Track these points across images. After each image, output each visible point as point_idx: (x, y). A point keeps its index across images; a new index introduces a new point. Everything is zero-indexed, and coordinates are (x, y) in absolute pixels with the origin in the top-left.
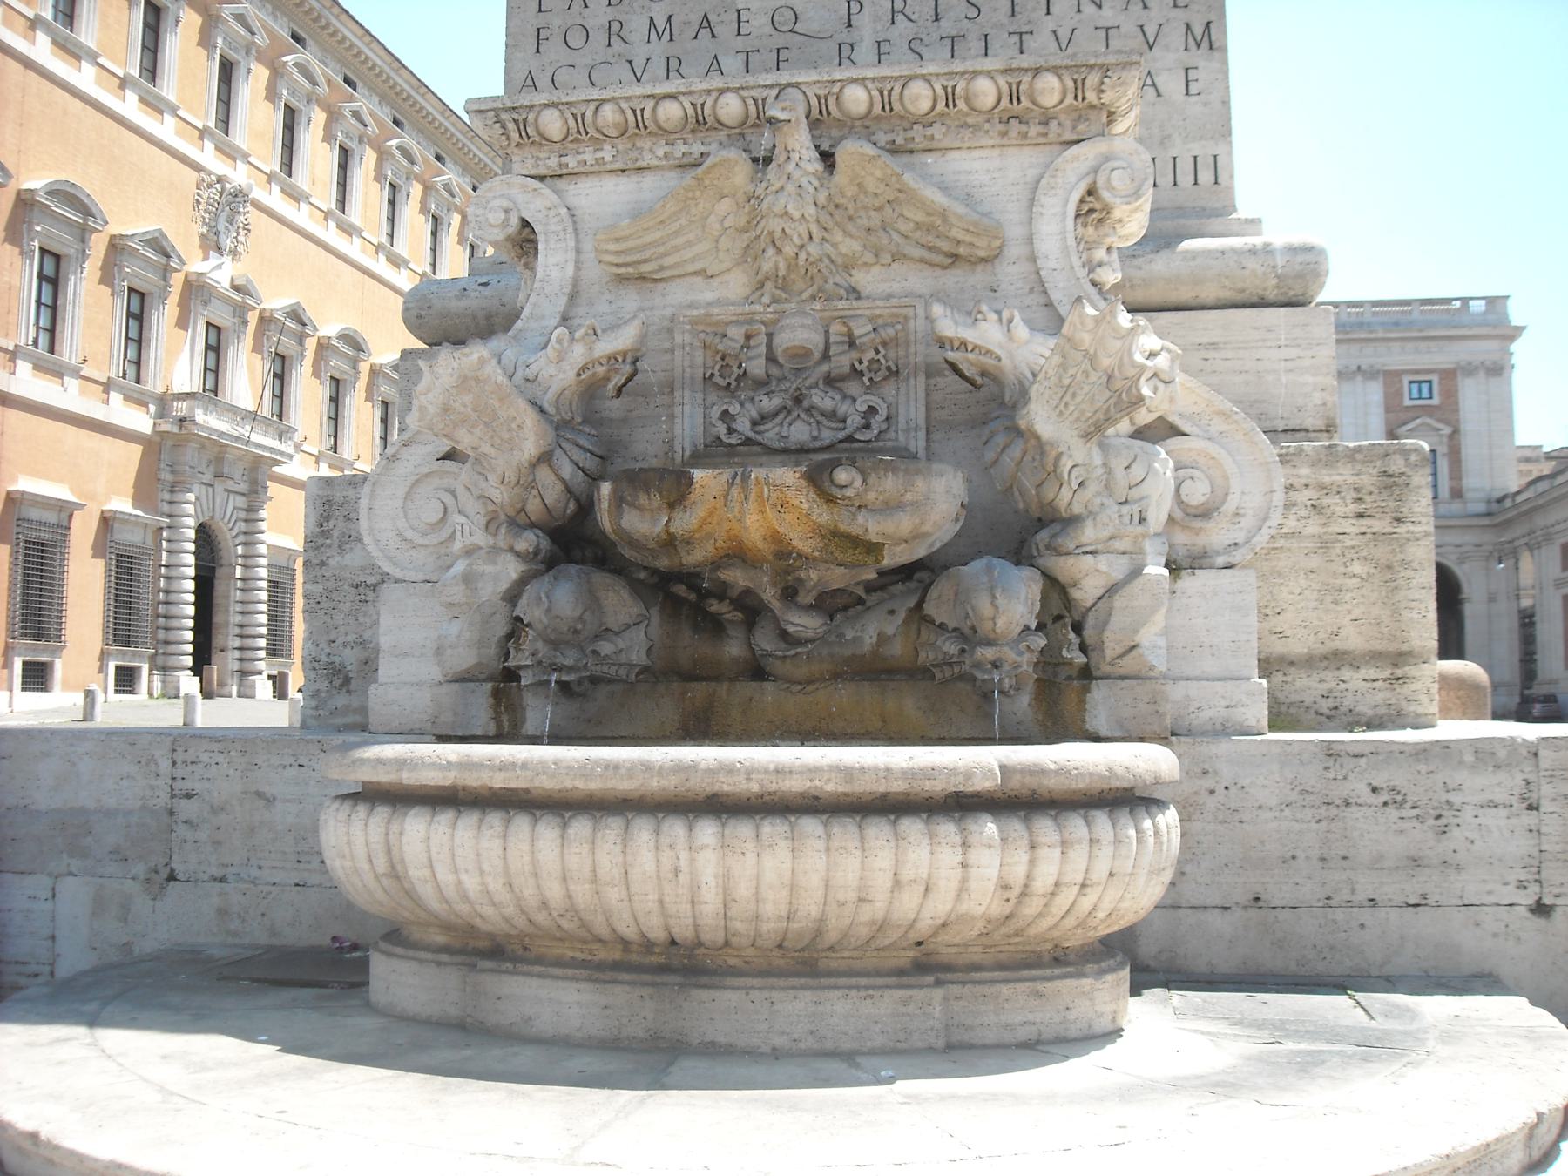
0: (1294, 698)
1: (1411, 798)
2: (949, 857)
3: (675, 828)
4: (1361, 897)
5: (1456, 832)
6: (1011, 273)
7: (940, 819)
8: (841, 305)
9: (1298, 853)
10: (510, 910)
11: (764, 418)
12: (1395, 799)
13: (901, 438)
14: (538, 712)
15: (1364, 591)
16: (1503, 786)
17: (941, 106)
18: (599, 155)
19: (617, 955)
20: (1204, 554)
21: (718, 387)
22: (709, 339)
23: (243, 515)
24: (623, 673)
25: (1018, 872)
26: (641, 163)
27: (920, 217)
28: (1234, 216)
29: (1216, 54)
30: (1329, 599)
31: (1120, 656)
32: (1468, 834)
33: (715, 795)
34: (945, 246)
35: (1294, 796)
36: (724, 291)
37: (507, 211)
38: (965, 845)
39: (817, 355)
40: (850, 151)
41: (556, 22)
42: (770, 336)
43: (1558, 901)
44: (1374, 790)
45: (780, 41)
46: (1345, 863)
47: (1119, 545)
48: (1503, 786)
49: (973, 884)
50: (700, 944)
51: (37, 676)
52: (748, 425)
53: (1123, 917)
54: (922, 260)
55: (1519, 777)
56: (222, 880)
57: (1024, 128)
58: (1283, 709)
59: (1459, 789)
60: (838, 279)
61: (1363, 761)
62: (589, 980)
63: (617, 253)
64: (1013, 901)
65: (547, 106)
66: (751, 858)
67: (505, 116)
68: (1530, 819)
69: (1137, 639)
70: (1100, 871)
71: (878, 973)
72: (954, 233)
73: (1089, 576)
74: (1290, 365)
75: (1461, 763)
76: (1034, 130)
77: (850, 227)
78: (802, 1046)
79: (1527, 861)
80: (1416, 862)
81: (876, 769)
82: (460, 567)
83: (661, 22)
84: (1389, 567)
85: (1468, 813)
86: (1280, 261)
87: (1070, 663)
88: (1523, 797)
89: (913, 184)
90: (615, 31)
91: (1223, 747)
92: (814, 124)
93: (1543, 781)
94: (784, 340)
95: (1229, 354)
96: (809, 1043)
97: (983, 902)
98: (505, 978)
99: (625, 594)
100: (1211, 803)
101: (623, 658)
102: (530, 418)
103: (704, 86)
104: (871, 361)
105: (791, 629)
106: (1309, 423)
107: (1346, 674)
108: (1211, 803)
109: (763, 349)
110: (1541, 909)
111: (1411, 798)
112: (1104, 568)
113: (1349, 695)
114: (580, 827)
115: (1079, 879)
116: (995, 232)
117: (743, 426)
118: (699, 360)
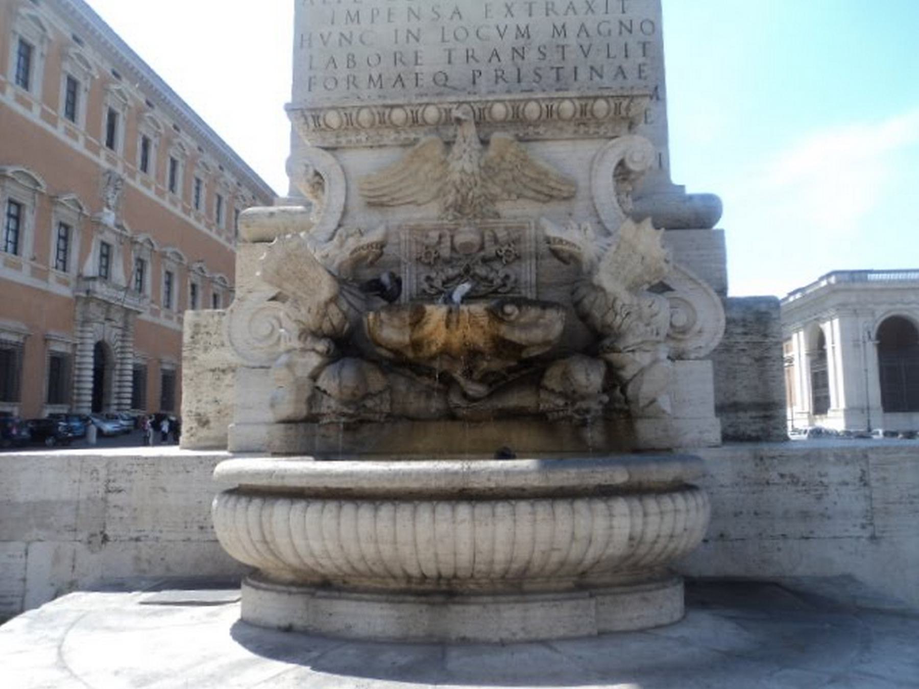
3: (444, 510)
6: (580, 206)
7: (596, 500)
10: (340, 562)
13: (523, 291)
18: (359, 137)
19: (403, 585)
21: (424, 264)
22: (419, 238)
23: (120, 338)
24: (377, 417)
25: (638, 529)
26: (382, 143)
33: (464, 489)
34: (545, 190)
36: (428, 214)
37: (307, 166)
39: (477, 247)
40: (497, 137)
42: (452, 237)
50: (455, 577)
52: (440, 284)
56: (137, 539)
57: (586, 129)
59: (826, 475)
61: (776, 461)
62: (387, 601)
63: (370, 190)
67: (307, 113)
72: (552, 184)
78: (518, 637)
82: (284, 359)
83: (375, 78)
85: (832, 489)
92: (477, 124)
97: (619, 547)
98: (335, 602)
103: (418, 101)
104: (507, 251)
105: (470, 393)
107: (741, 414)
109: (449, 244)
111: (803, 480)
114: (386, 511)
116: (573, 183)
117: (438, 283)
118: (414, 248)
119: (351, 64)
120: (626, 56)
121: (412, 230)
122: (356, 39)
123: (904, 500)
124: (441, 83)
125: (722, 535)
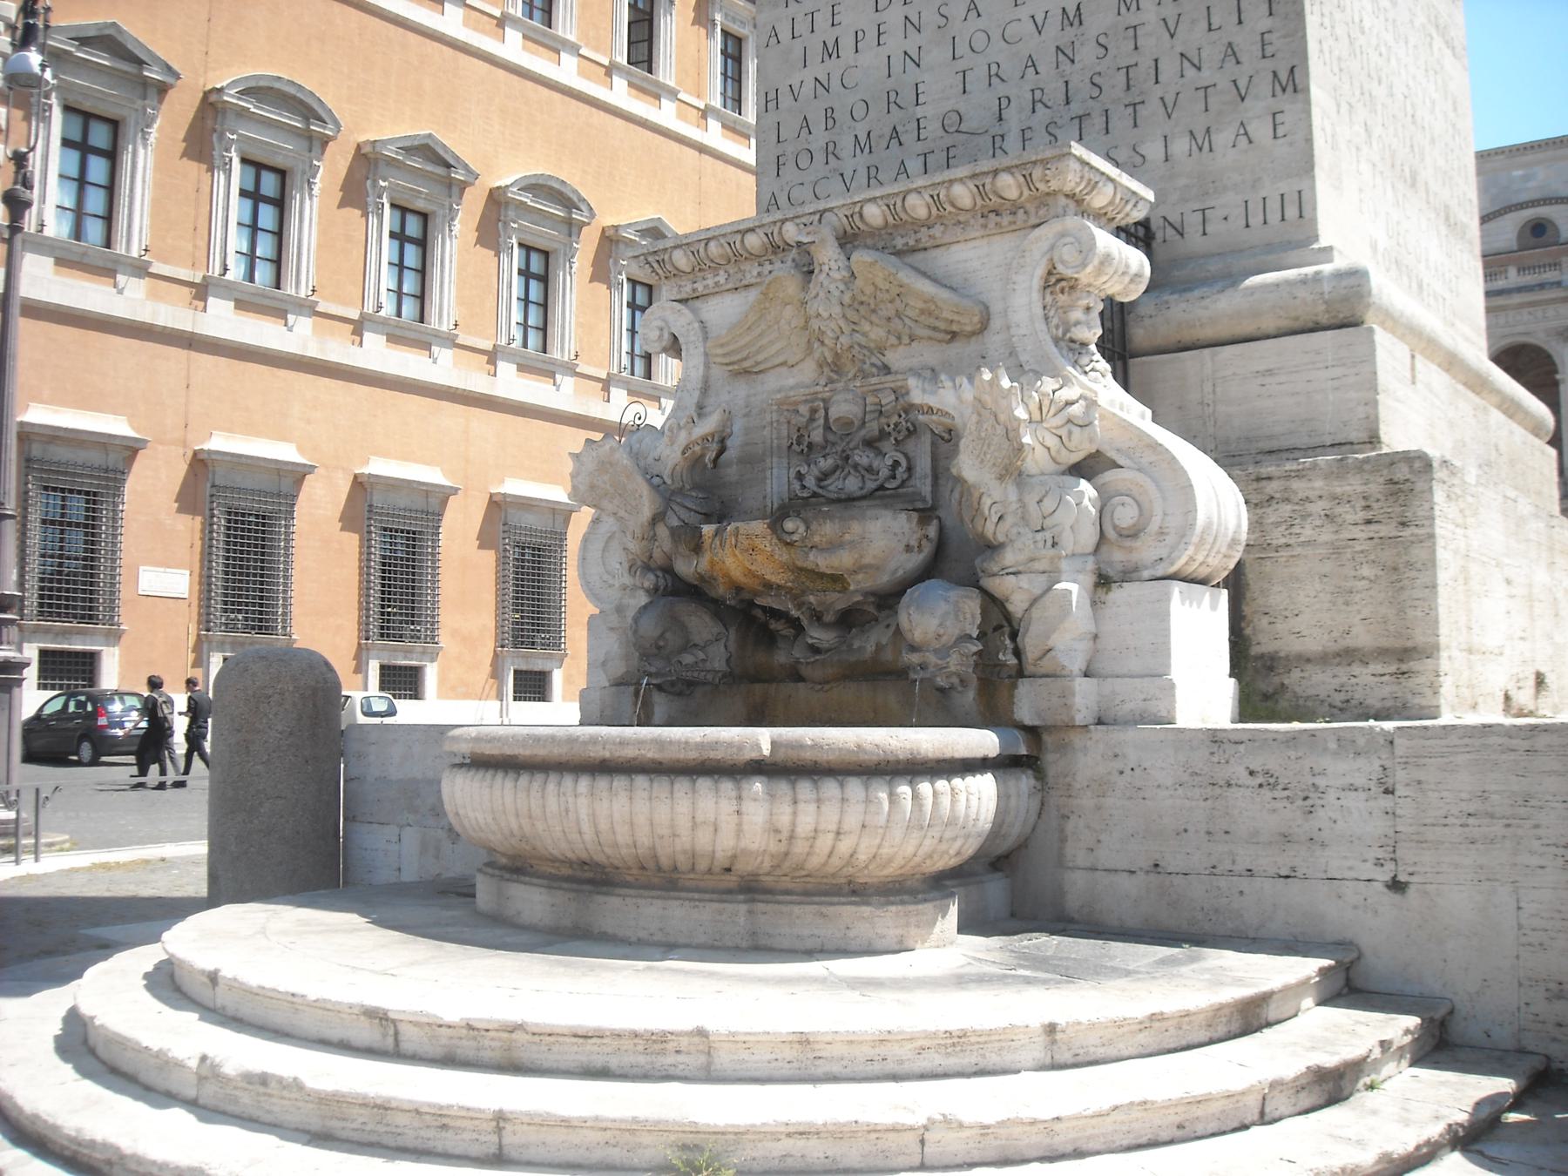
0: (1311, 692)
1: (1283, 781)
2: (727, 807)
4: (1240, 867)
5: (1321, 813)
8: (874, 380)
9: (1189, 827)
11: (824, 476)
12: (1269, 782)
14: (659, 711)
15: (1371, 592)
16: (1363, 770)
17: (934, 211)
20: (1136, 569)
24: (710, 677)
27: (920, 305)
28: (1315, 246)
29: (1300, 96)
30: (1340, 600)
31: (1040, 659)
32: (1331, 814)
34: (942, 325)
35: (1185, 778)
38: (739, 798)
39: (857, 423)
41: (790, 149)
43: (1412, 879)
44: (1252, 773)
45: (949, 141)
46: (1227, 837)
47: (1037, 566)
48: (1363, 770)
49: (745, 827)
51: (533, 686)
53: (890, 860)
54: (930, 338)
55: (1377, 764)
57: (998, 219)
58: (1301, 702)
59: (1323, 773)
60: (874, 360)
61: (1241, 748)
63: (725, 355)
64: (784, 842)
65: (675, 247)
66: (605, 803)
68: (1386, 802)
69: (1050, 643)
70: (853, 820)
71: (713, 892)
73: (1016, 591)
74: (1336, 383)
75: (1326, 749)
76: (1006, 219)
77: (874, 318)
79: (1384, 841)
80: (1286, 838)
81: (679, 742)
83: (863, 138)
84: (1395, 569)
85: (1331, 796)
86: (1326, 288)
87: (1004, 665)
88: (1380, 782)
89: (906, 281)
90: (831, 151)
91: (1130, 734)
93: (1398, 768)
94: (834, 413)
95: (1283, 378)
96: (658, 937)
99: (707, 618)
100: (1121, 782)
101: (708, 666)
102: (645, 490)
103: (771, 219)
106: (1354, 436)
107: (1357, 669)
108: (1121, 782)
109: (822, 421)
110: (1396, 886)
111: (1283, 781)
112: (1025, 586)
113: (1359, 689)
115: (834, 827)
117: (810, 482)
119: (830, 122)
120: (1240, 22)
121: (780, 403)
122: (835, 84)
123: (1450, 820)
124: (952, 130)
125: (1157, 865)
